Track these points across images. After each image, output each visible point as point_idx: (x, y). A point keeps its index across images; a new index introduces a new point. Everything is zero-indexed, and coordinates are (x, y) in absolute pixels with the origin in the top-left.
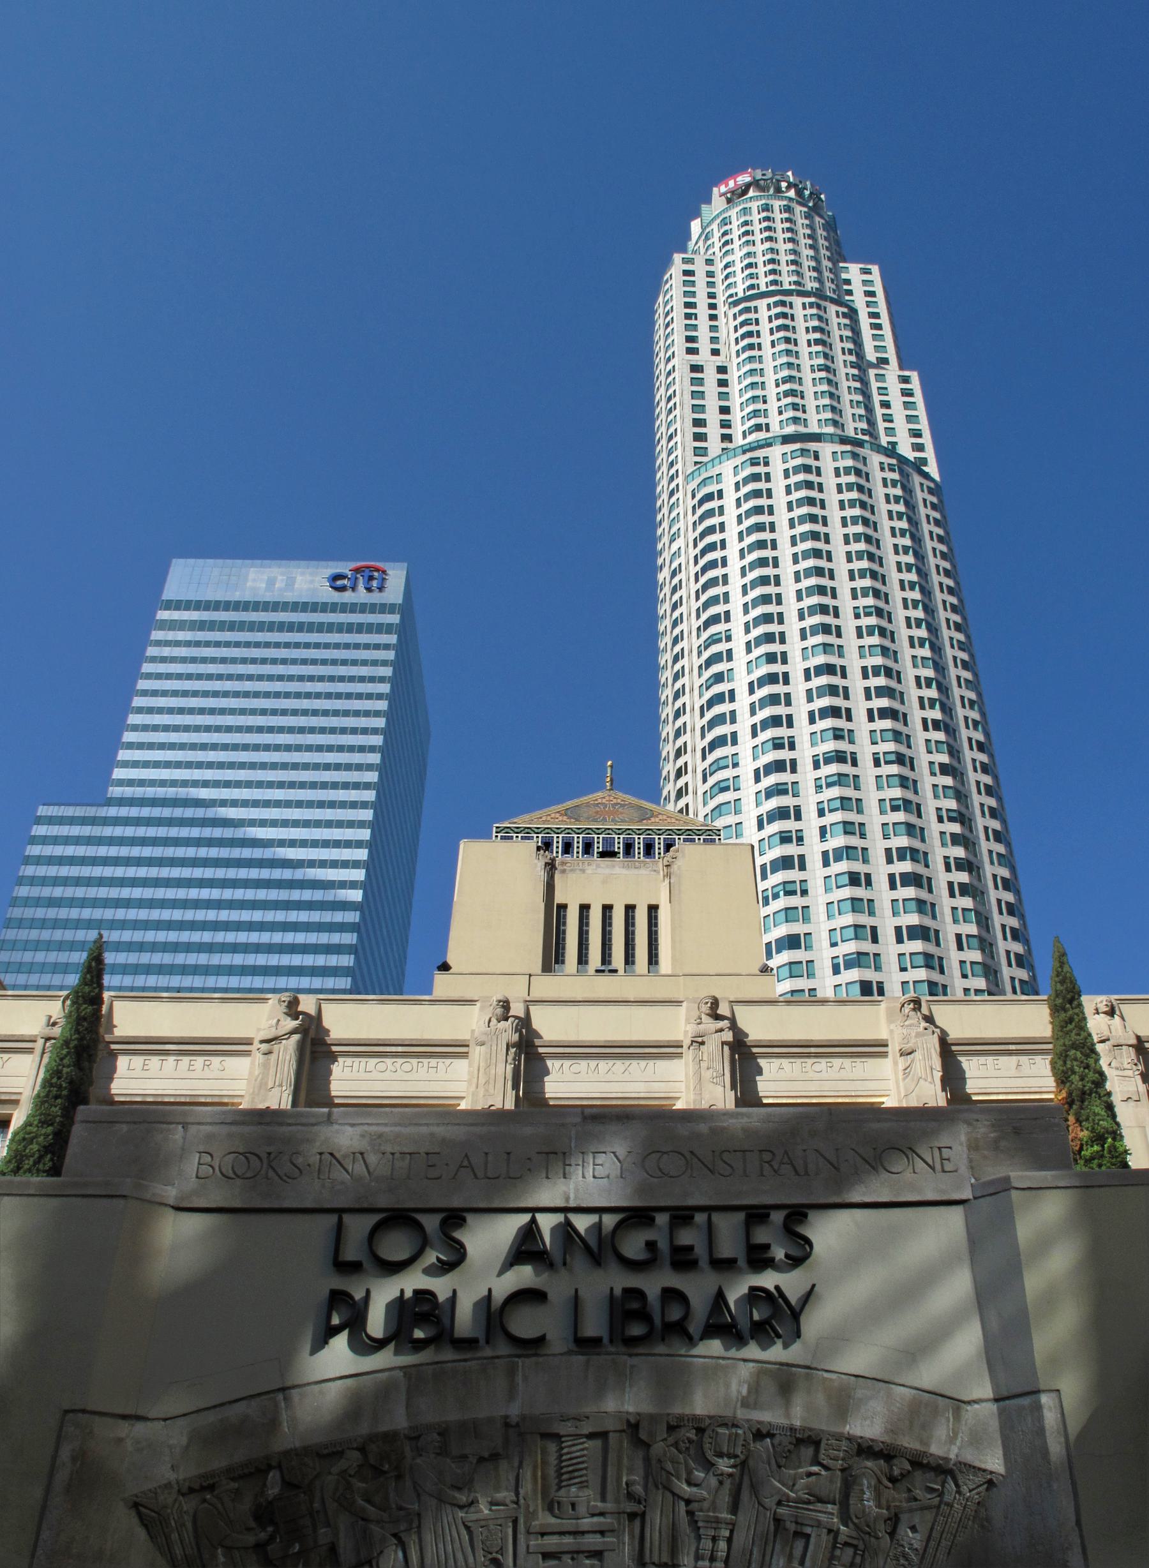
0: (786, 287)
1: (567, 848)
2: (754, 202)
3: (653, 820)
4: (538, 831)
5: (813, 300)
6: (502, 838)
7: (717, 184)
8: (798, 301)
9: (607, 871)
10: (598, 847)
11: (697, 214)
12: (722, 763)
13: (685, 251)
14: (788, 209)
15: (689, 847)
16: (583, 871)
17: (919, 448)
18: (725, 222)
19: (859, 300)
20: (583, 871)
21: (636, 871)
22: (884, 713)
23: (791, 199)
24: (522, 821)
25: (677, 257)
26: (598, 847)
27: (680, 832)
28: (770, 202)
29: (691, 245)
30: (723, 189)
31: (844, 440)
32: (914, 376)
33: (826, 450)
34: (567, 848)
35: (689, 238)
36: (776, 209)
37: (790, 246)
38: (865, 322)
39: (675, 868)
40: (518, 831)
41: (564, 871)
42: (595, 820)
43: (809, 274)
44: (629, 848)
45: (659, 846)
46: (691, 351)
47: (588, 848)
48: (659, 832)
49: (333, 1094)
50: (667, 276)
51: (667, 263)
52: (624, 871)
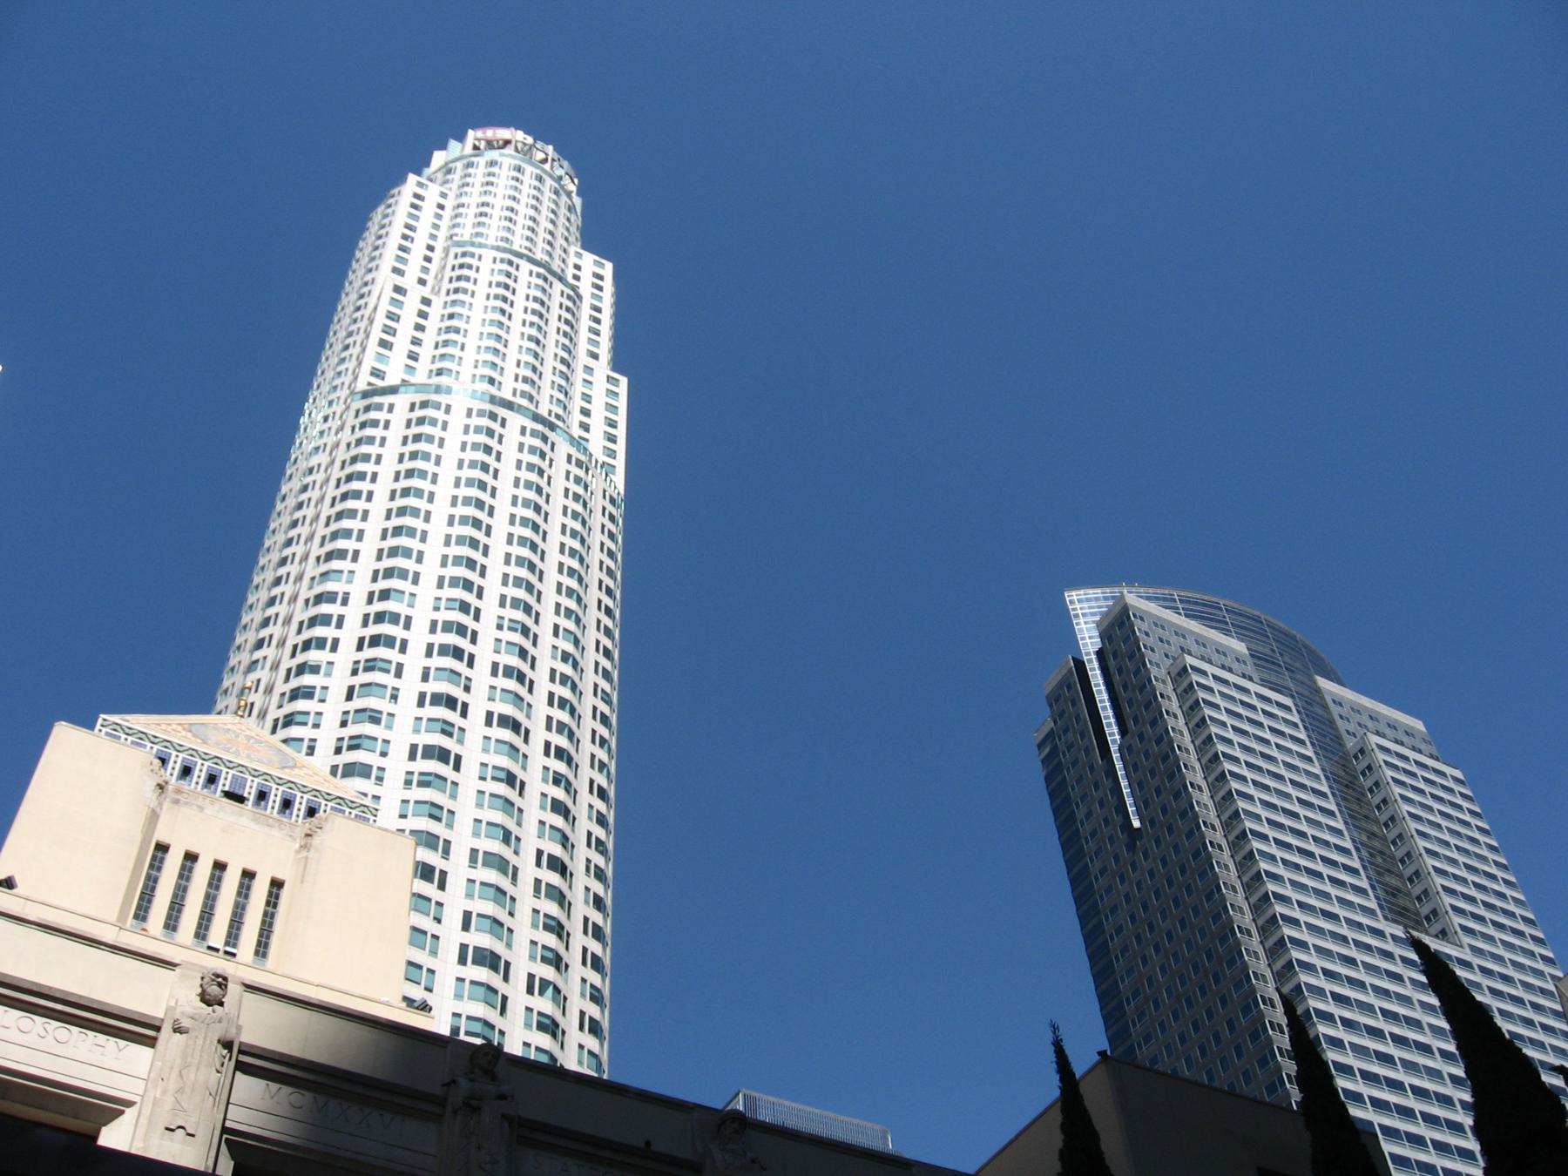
0: (516, 247)
1: (186, 771)
2: (507, 158)
3: (296, 771)
4: (154, 740)
5: (542, 271)
6: (107, 734)
7: (476, 126)
8: (526, 267)
9: (233, 819)
10: (224, 784)
11: (443, 147)
12: (298, 718)
13: (419, 173)
14: (540, 179)
15: (339, 820)
16: (201, 809)
17: (612, 454)
18: (470, 165)
19: (585, 288)
20: (201, 809)
21: (267, 829)
22: (505, 721)
23: (545, 171)
24: (138, 721)
25: (412, 178)
26: (224, 784)
27: (328, 797)
28: (523, 165)
29: (428, 172)
30: (480, 134)
31: (537, 418)
32: (624, 381)
33: (515, 421)
34: (186, 771)
35: (428, 165)
36: (528, 174)
37: (532, 212)
38: (585, 311)
39: (316, 841)
40: (129, 732)
41: (177, 802)
42: (227, 750)
43: (541, 245)
44: (262, 796)
45: (300, 807)
46: (398, 272)
47: (212, 779)
48: (304, 789)
49: (720, 1107)
50: (395, 191)
51: (401, 180)
52: (253, 825)
